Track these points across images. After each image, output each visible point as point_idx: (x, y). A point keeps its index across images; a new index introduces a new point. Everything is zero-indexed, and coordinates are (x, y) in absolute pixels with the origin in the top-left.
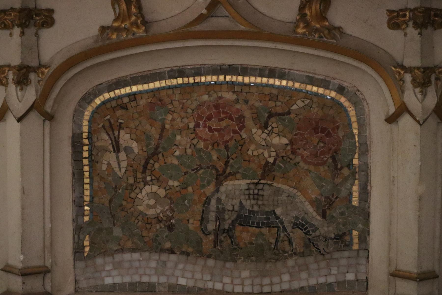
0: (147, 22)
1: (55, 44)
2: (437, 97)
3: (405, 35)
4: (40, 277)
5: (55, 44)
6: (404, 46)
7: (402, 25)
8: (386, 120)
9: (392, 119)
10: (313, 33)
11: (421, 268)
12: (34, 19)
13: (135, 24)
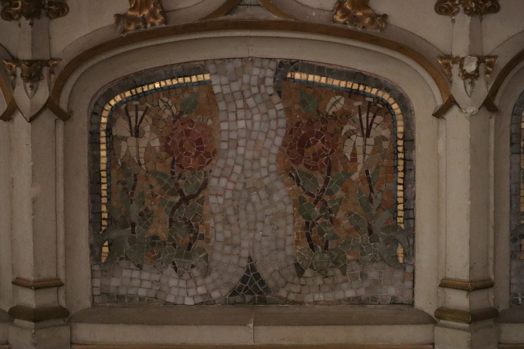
1: (67, 36)
2: (50, 90)
3: (20, 25)
4: (55, 289)
5: (67, 36)
6: (451, 35)
7: (15, 15)
11: (39, 276)
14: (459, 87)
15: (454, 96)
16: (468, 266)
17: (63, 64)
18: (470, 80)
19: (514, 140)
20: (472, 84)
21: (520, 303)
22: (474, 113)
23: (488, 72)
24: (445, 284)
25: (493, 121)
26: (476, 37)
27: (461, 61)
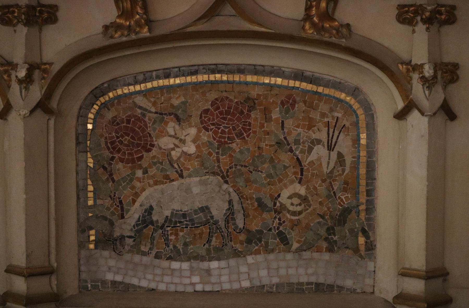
0: (151, 21)
1: (59, 43)
6: (414, 45)
8: (394, 117)
9: (401, 116)
10: (360, 271)
12: (41, 16)
13: (138, 24)
14: (418, 91)
15: (10, 100)
16: (25, 254)
17: (55, 69)
18: (25, 85)
19: (80, 140)
20: (27, 89)
21: (89, 289)
22: (26, 116)
23: (44, 78)
24: (405, 273)
25: (52, 122)
26: (434, 47)
27: (418, 68)
